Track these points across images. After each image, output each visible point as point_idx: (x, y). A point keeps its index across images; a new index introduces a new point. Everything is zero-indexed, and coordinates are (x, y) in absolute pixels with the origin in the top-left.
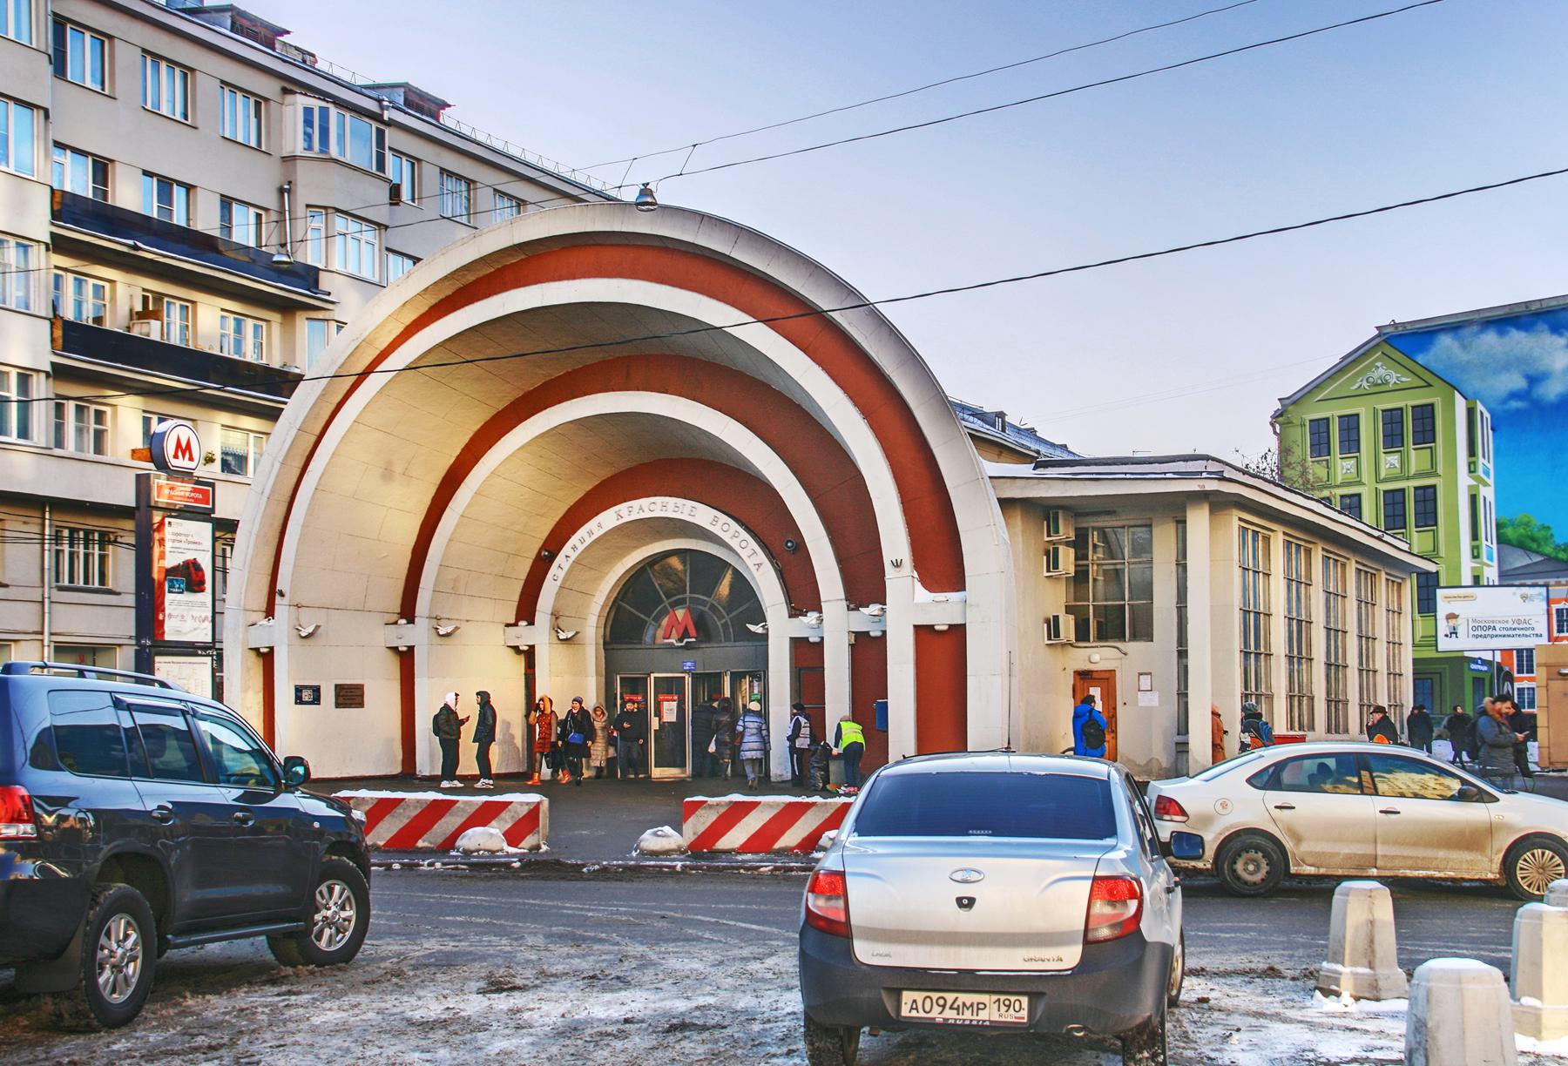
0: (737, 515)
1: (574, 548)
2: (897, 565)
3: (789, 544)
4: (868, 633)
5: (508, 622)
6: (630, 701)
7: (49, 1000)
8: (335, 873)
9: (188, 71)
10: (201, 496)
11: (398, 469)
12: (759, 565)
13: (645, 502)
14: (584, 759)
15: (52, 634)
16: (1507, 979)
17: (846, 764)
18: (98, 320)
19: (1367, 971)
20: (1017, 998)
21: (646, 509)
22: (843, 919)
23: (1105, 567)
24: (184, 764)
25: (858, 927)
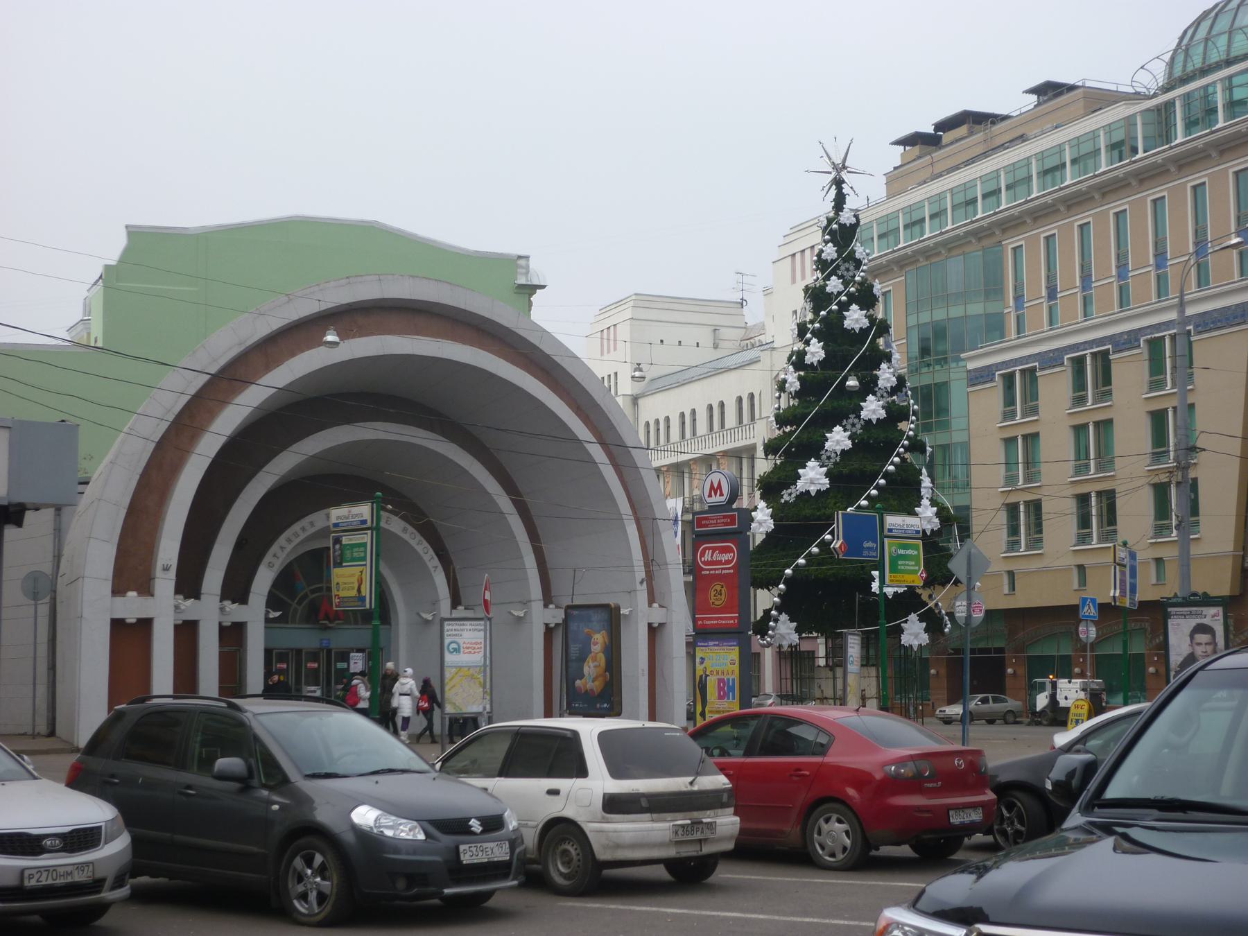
1: (289, 541)
6: (750, 663)
8: (784, 652)
10: (731, 684)
12: (282, 548)
15: (365, 565)
16: (37, 509)
18: (956, 812)
19: (1083, 746)
20: (481, 844)
22: (1123, 121)
23: (290, 653)
25: (632, 390)
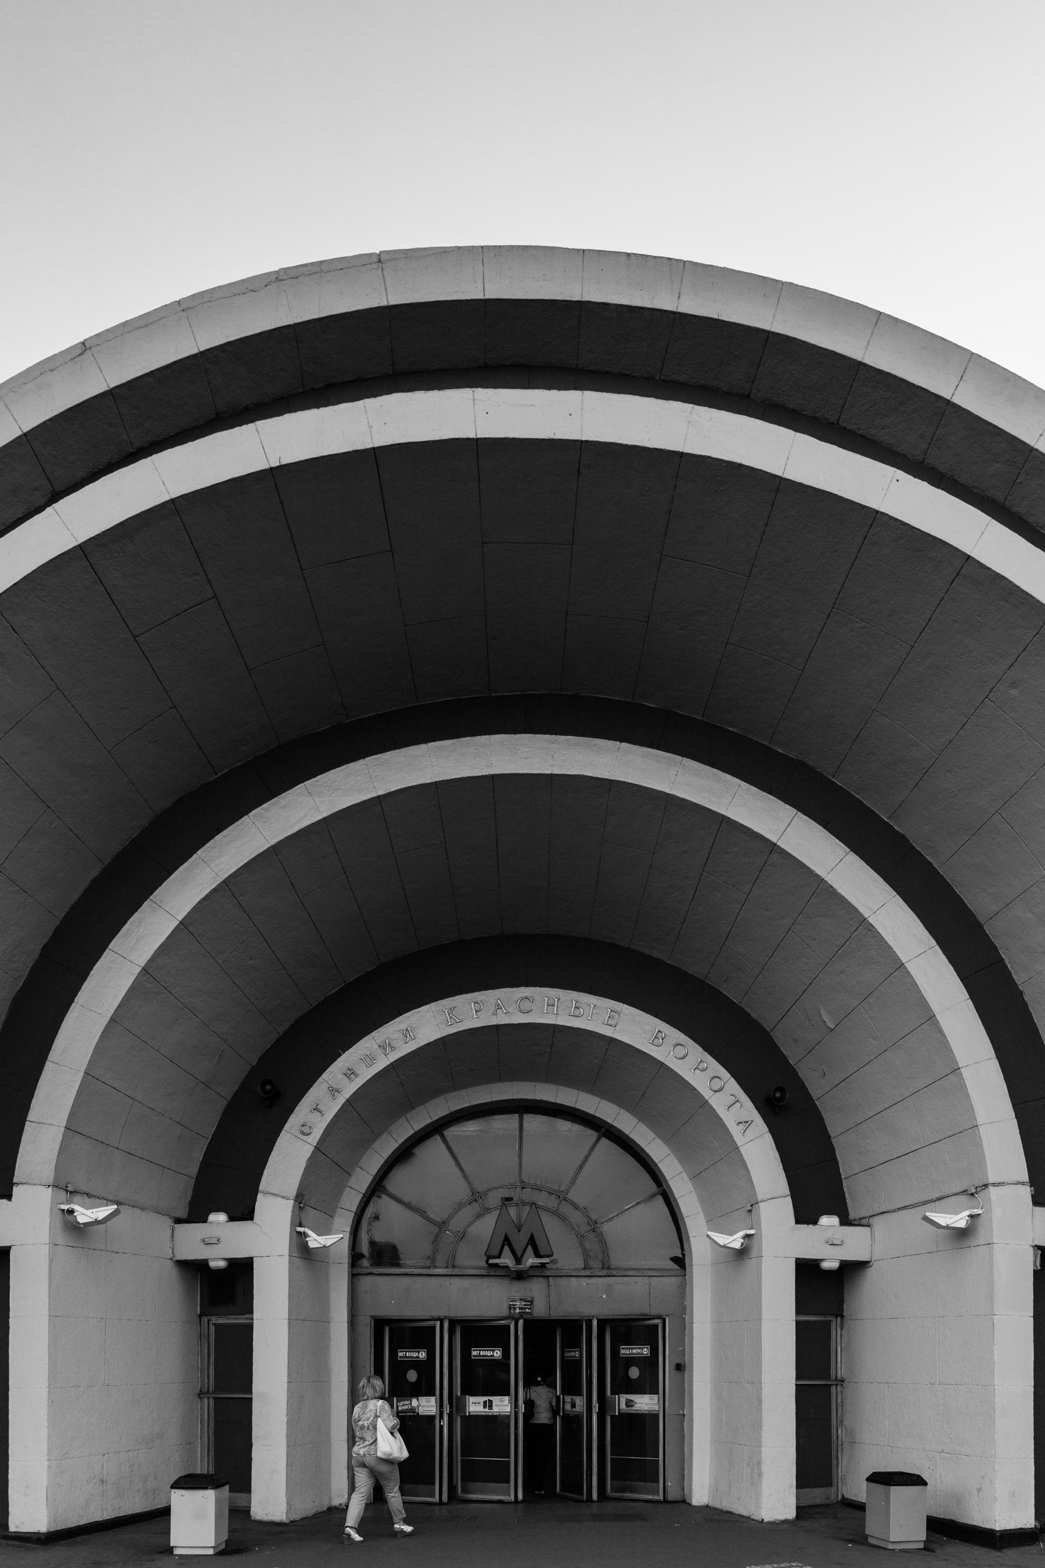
0: (81, 474)
2: (489, 1405)
3: (268, 1087)
4: (232, 1219)
5: (178, 1216)
7: (356, 1449)
9: (453, 1242)
11: (497, 254)
13: (334, 1072)
14: (395, 1398)
17: (12, 1182)
21: (315, 1117)
24: (531, 1422)
